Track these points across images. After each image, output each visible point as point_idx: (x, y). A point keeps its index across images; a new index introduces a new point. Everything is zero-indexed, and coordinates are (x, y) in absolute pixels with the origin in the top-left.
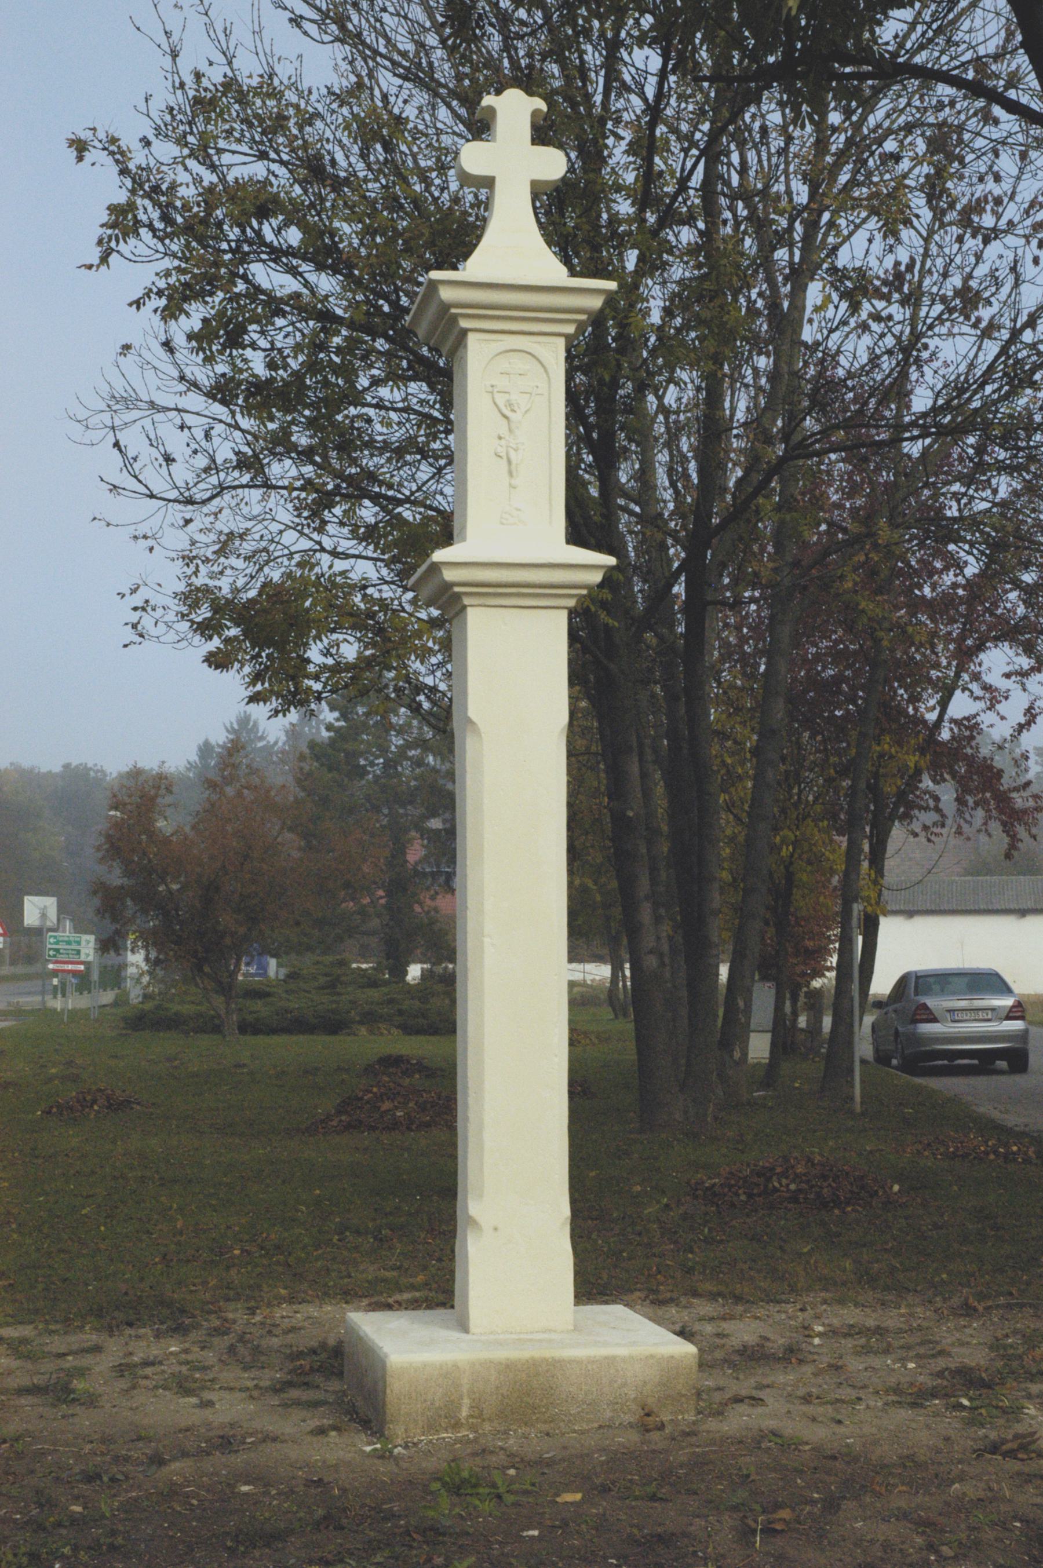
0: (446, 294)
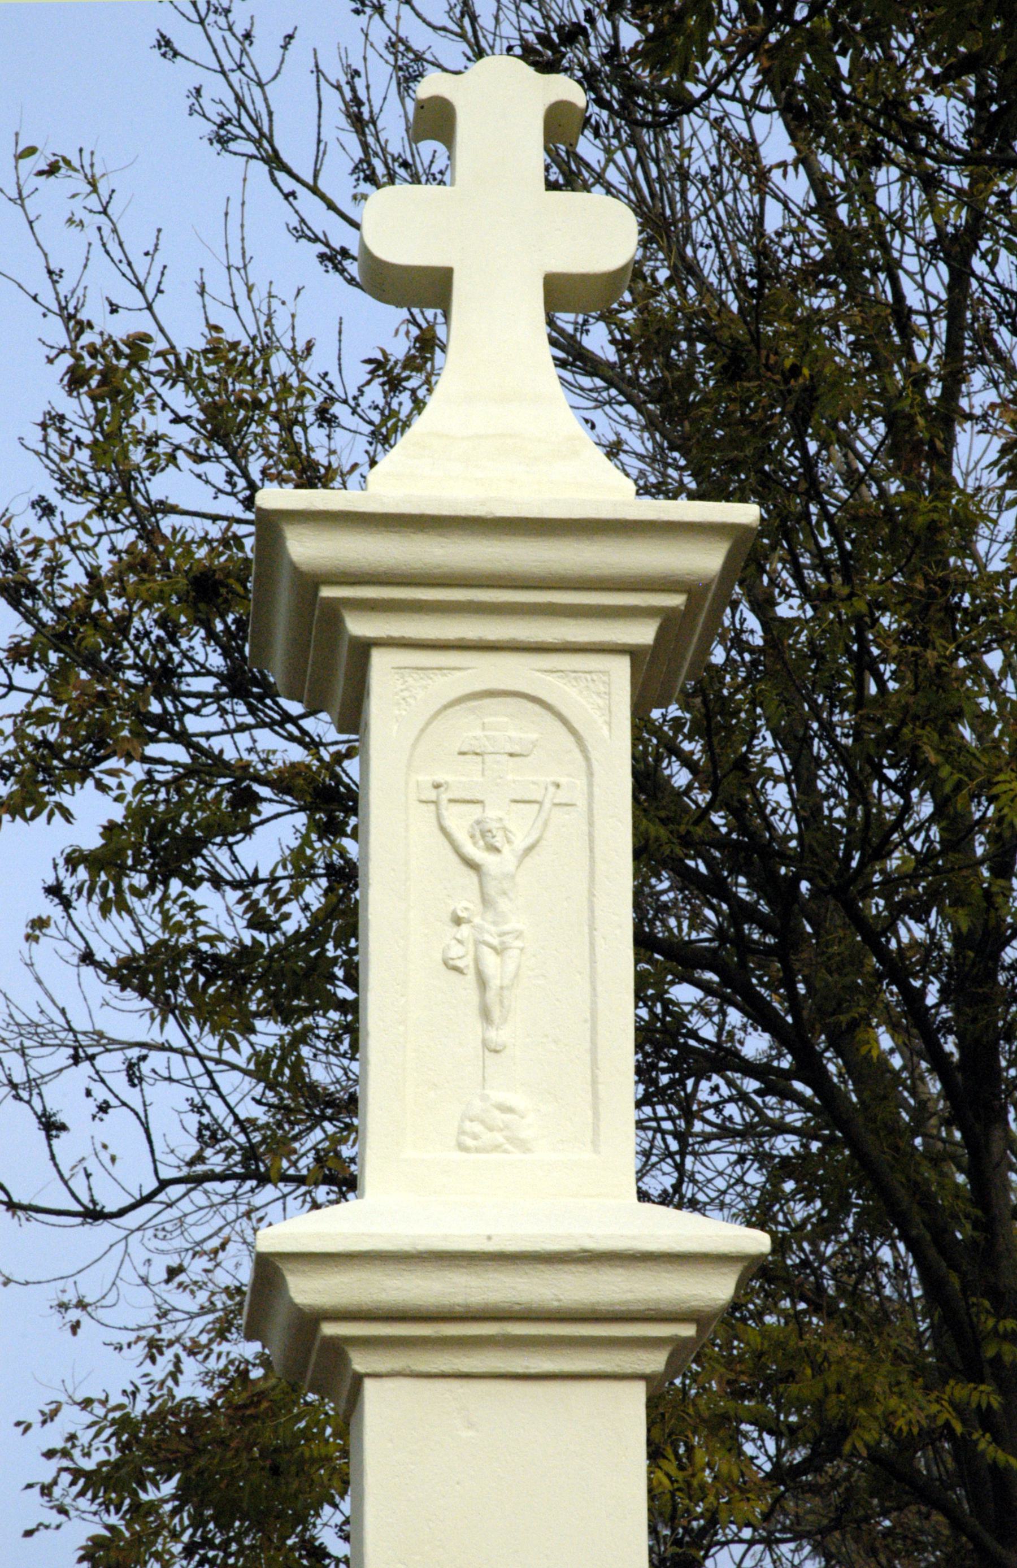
0: (304, 548)
